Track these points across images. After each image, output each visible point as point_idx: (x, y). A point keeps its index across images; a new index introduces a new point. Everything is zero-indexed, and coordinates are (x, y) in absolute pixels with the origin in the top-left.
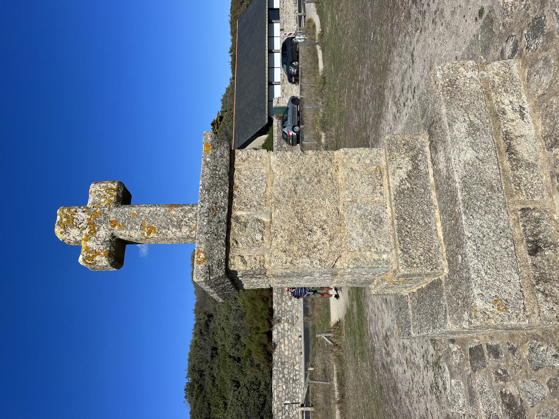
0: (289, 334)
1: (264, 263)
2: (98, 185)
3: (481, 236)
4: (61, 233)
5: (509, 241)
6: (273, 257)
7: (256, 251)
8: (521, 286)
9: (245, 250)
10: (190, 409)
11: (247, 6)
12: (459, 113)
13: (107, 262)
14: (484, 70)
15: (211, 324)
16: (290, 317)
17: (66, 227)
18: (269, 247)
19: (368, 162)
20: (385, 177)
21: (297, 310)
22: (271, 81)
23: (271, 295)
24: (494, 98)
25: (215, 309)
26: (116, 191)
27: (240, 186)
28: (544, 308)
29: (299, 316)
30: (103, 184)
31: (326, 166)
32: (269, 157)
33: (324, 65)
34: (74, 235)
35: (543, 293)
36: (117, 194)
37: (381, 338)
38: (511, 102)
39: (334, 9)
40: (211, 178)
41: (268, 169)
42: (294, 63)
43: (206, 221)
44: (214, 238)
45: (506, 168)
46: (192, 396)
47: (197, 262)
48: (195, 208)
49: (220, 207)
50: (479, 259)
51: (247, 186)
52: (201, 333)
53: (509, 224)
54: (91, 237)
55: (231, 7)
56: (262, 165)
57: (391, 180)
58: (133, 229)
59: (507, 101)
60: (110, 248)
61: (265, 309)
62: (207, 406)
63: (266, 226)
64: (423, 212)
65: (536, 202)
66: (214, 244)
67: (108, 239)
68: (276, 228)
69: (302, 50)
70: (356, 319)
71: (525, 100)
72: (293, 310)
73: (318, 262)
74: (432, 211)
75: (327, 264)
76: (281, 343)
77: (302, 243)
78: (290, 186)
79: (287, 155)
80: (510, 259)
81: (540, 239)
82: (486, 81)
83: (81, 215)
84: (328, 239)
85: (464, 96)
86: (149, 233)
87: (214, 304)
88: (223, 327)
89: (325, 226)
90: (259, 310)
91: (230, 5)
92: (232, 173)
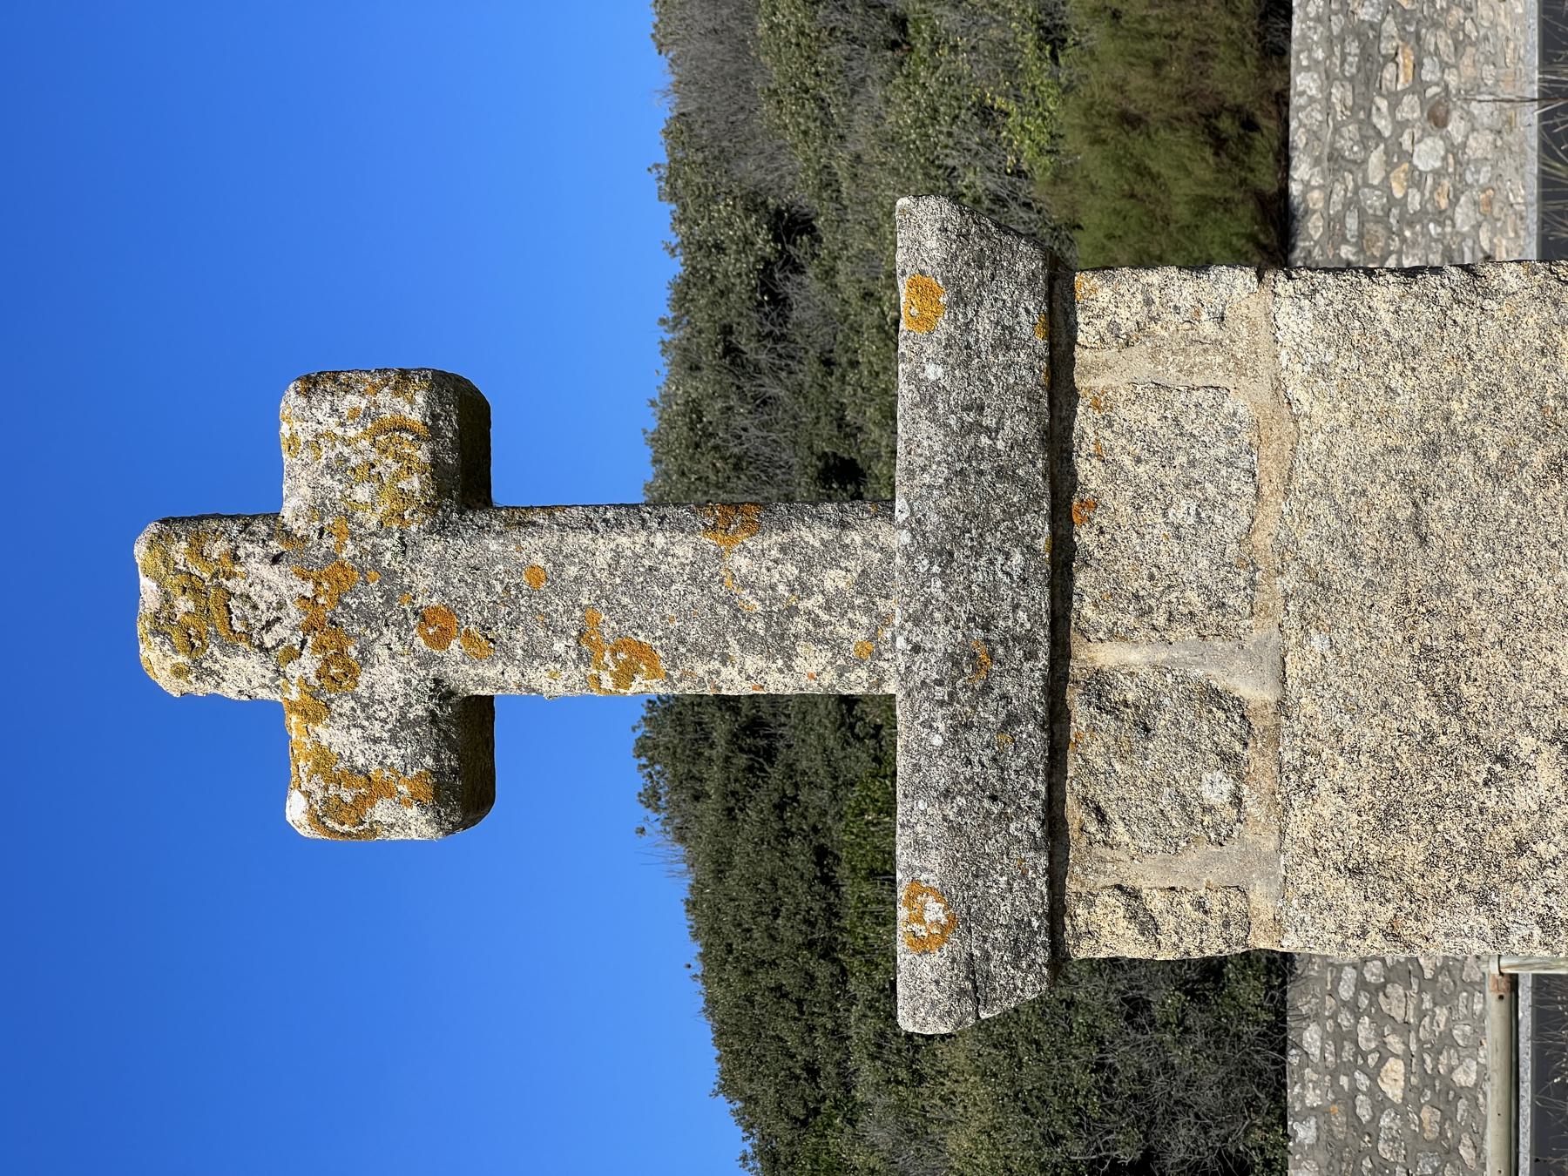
1: (1248, 928)
2: (326, 406)
6: (1295, 902)
7: (1205, 864)
9: (1149, 859)
10: (689, 880)
17: (197, 643)
18: (1271, 844)
23: (1278, 87)
25: (828, 183)
26: (427, 440)
27: (1107, 499)
36: (433, 452)
41: (1264, 389)
43: (942, 727)
44: (989, 813)
46: (696, 798)
47: (910, 944)
48: (858, 540)
51: (1146, 499)
52: (731, 351)
54: (332, 701)
56: (1231, 365)
58: (539, 656)
60: (437, 759)
62: (810, 869)
63: (1257, 725)
67: (418, 711)
68: (1311, 744)
72: (1454, 202)
73: (1537, 931)
77: (1452, 825)
78: (1391, 498)
79: (1374, 304)
92: (1062, 420)
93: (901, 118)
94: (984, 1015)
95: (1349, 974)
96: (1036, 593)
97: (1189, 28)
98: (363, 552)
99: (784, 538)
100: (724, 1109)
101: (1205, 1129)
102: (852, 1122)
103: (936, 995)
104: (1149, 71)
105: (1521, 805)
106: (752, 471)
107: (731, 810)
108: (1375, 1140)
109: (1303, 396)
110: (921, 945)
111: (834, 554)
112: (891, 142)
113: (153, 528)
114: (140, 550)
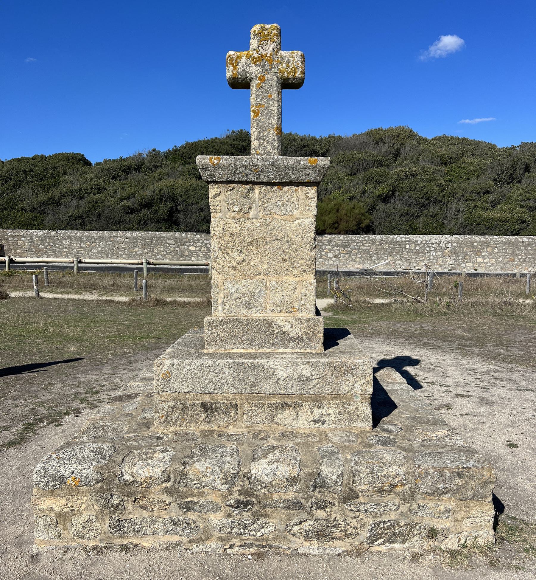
2: (299, 59)
3: (216, 371)
5: (212, 390)
8: (179, 392)
9: (225, 197)
10: (220, 138)
14: (362, 399)
18: (227, 216)
19: (303, 302)
20: (287, 314)
21: (323, 264)
23: (341, 233)
24: (334, 402)
27: (281, 191)
28: (164, 404)
31: (299, 267)
32: (309, 217)
36: (291, 78)
38: (329, 415)
40: (284, 166)
41: (298, 216)
44: (232, 171)
46: (233, 139)
50: (199, 367)
52: (304, 146)
53: (226, 393)
57: (281, 318)
60: (240, 78)
63: (246, 215)
64: (252, 341)
67: (248, 75)
68: (243, 223)
71: (330, 426)
72: (323, 259)
74: (254, 347)
78: (281, 236)
80: (199, 389)
81: (213, 413)
84: (234, 265)
85: (336, 378)
86: (254, 112)
89: (245, 263)
93: (340, 174)
94: (200, 170)
95: (208, 242)
96: (267, 180)
97: (351, 219)
98: (274, 65)
99: (276, 139)
100: (184, 143)
101: (183, 220)
102: (182, 164)
103: (202, 162)
104: (345, 213)
105: (234, 254)
106: (285, 150)
107: (231, 145)
108: (183, 245)
109: (296, 223)
110: (210, 160)
111: (273, 147)
112: (336, 173)
113: (279, 27)
114: (275, 25)
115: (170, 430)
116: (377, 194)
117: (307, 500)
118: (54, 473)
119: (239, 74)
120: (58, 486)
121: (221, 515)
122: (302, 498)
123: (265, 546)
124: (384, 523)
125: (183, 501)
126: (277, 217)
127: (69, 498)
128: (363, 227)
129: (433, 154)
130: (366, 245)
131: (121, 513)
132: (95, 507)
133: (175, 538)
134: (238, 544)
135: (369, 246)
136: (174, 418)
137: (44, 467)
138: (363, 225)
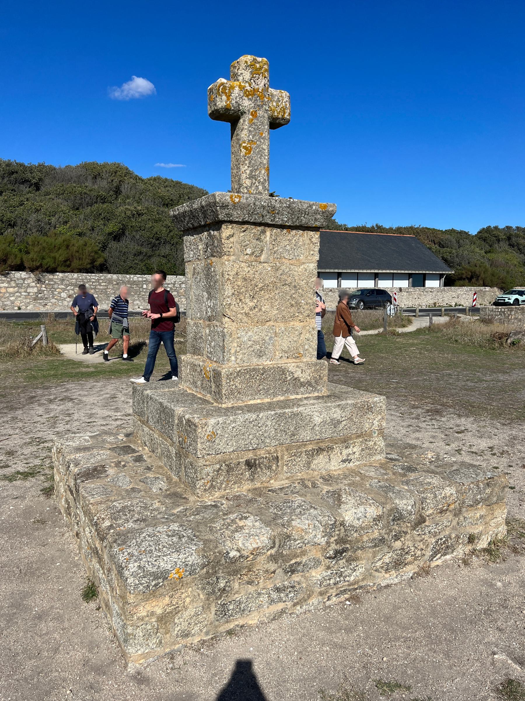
0: (22, 294)
3: (260, 425)
4: (246, 62)
5: (256, 446)
7: (237, 248)
11: (430, 249)
12: (347, 413)
13: (220, 106)
14: (378, 434)
15: (26, 188)
16: (45, 295)
18: (241, 260)
19: (306, 347)
20: (294, 360)
22: (342, 275)
25: (48, 194)
28: (209, 469)
29: (47, 307)
30: (288, 105)
33: (362, 336)
34: (244, 75)
35: (220, 469)
37: (65, 394)
38: (354, 453)
39: (422, 345)
42: (362, 303)
45: (307, 447)
49: (275, 217)
52: (13, 173)
53: (268, 446)
55: (429, 229)
57: (293, 364)
59: (355, 450)
61: (55, 262)
65: (283, 467)
66: (245, 211)
67: (241, 108)
69: (377, 313)
70: (74, 371)
71: (355, 463)
72: (56, 299)
74: (269, 397)
75: (227, 310)
76: (9, 282)
78: (289, 280)
80: (243, 446)
81: (257, 469)
82: (370, 435)
83: (262, 82)
84: (247, 312)
86: (245, 148)
87: (55, 192)
88: (24, 204)
89: (257, 309)
90: (52, 255)
91: (431, 227)
97: (84, 257)
104: (77, 250)
115: (216, 496)
116: (107, 232)
117: (388, 534)
118: (155, 569)
119: (233, 106)
120: (161, 584)
121: (321, 569)
122: (385, 534)
123: (356, 589)
124: (441, 539)
125: (288, 564)
126: (286, 261)
127: (173, 595)
128: (98, 265)
129: (154, 194)
130: (102, 284)
131: (227, 596)
132: (201, 596)
133: (280, 606)
134: (334, 594)
135: (105, 285)
136: (219, 482)
137: (139, 566)
138: (97, 263)
